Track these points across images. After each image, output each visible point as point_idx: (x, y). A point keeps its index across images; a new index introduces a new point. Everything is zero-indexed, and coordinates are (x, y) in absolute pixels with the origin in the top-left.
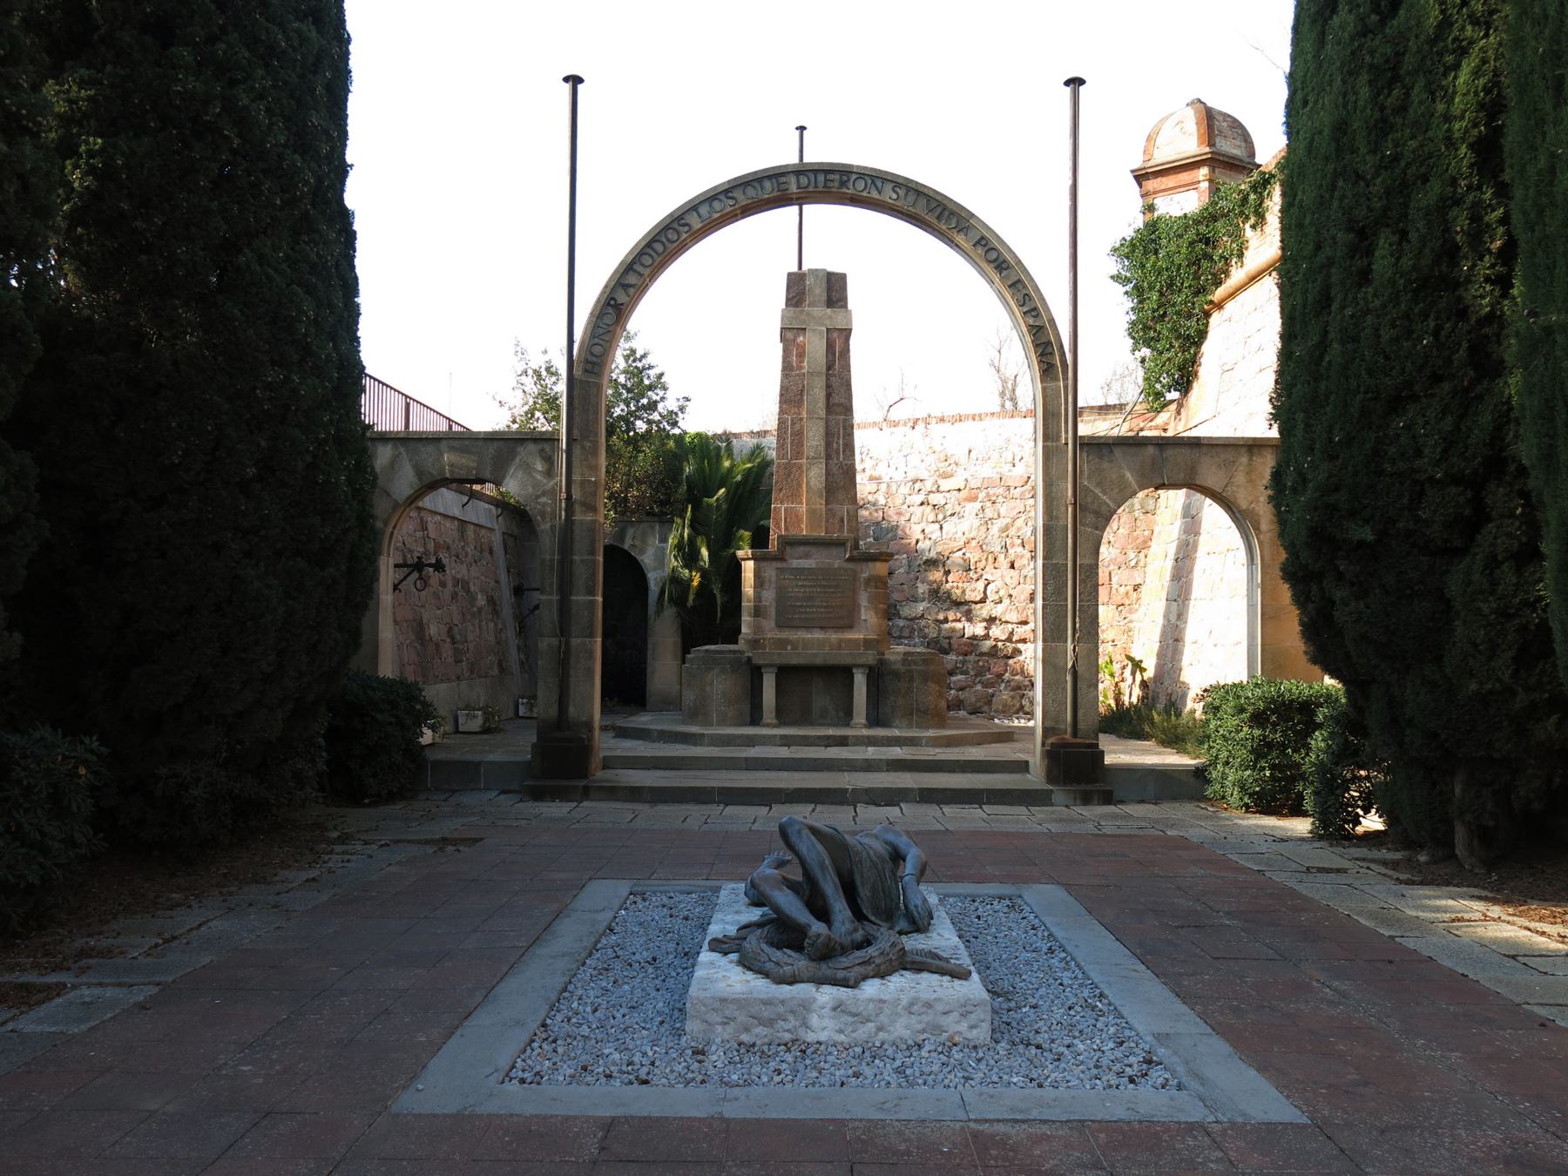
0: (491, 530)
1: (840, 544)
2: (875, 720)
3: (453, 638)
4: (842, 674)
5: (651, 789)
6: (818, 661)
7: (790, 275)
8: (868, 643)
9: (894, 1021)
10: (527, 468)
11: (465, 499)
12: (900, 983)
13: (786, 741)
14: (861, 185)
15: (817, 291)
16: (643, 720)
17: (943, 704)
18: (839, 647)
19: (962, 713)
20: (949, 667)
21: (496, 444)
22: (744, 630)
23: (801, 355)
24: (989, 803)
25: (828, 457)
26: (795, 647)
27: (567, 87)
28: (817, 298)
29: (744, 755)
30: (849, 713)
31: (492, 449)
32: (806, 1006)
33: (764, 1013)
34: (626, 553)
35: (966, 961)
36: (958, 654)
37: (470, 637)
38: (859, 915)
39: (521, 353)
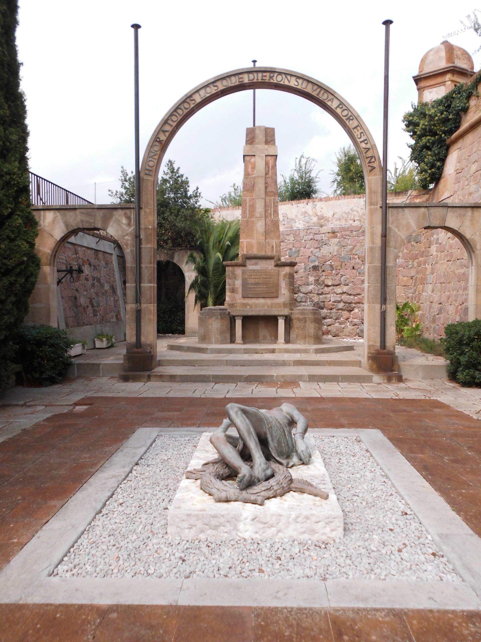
0: (111, 254)
1: (271, 258)
2: (287, 341)
4: (272, 320)
5: (180, 376)
6: (262, 313)
7: (247, 129)
8: (285, 305)
9: (287, 527)
10: (119, 223)
11: (98, 239)
12: (291, 498)
13: (246, 351)
14: (279, 78)
15: (261, 137)
16: (182, 341)
17: (321, 333)
18: (272, 307)
19: (330, 337)
20: (324, 315)
21: (103, 211)
22: (227, 299)
23: (253, 168)
24: (342, 382)
25: (266, 217)
26: (251, 307)
27: (133, 30)
28: (260, 138)
29: (225, 359)
30: (276, 337)
31: (101, 213)
32: (235, 520)
33: (212, 523)
34: (175, 265)
35: (327, 487)
36: (328, 309)
37: (102, 304)
38: (268, 457)
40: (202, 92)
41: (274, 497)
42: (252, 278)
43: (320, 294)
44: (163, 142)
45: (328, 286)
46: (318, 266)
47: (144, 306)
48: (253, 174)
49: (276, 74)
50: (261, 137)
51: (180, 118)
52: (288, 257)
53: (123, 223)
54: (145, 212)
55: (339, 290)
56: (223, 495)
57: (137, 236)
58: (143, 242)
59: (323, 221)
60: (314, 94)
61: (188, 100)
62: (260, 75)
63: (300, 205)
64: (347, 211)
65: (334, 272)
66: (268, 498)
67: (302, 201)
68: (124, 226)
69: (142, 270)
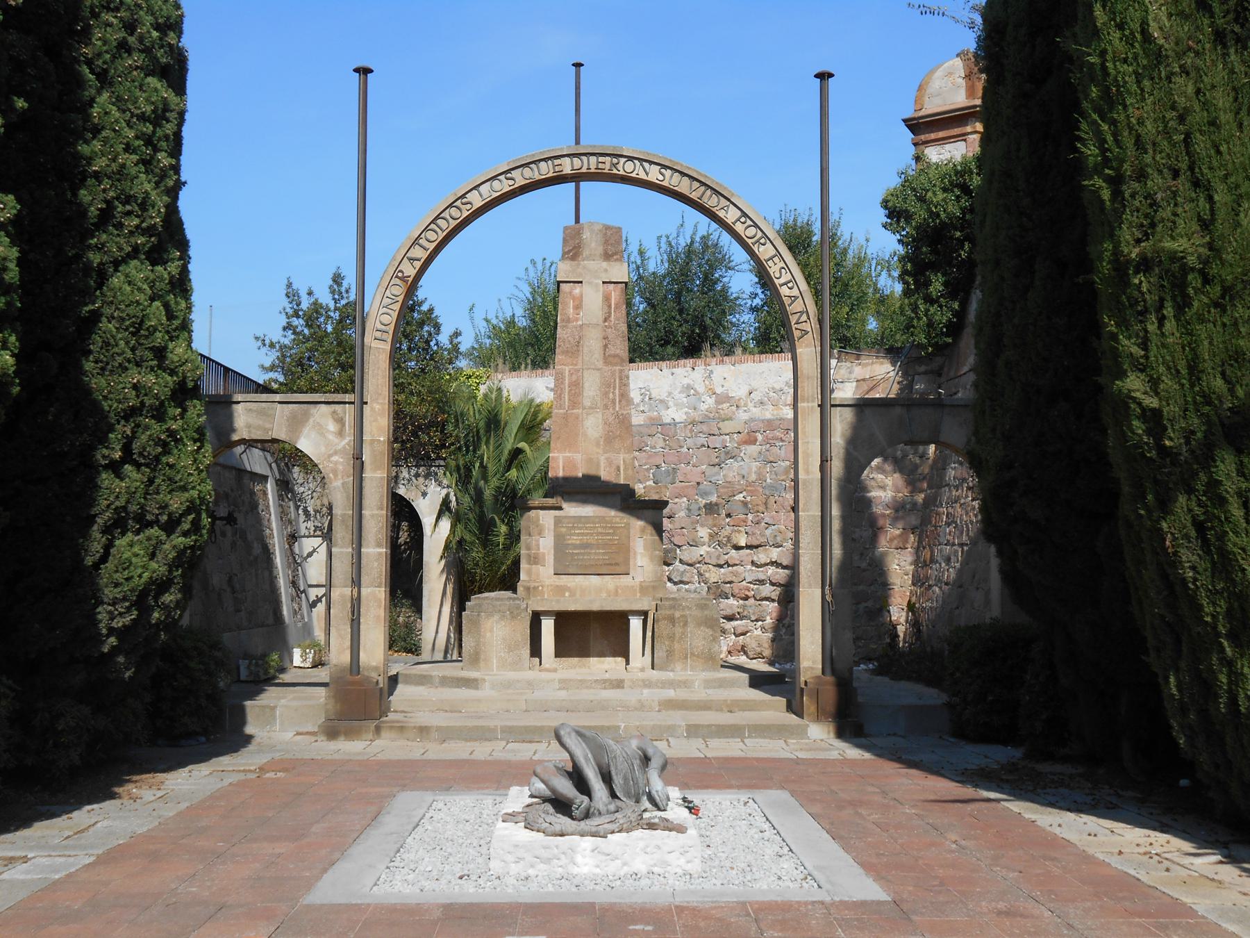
3: (233, 588)
6: (595, 607)
7: (566, 228)
8: (644, 589)
10: (320, 429)
26: (573, 594)
38: (613, 795)
39: (292, 295)
40: (485, 189)
41: (619, 831)
42: (575, 534)
43: (721, 566)
44: (410, 280)
45: (737, 548)
46: (716, 504)
47: (364, 591)
48: (577, 320)
49: (623, 160)
50: (593, 245)
51: (442, 235)
52: (651, 483)
53: (328, 431)
54: (372, 409)
55: (761, 557)
56: (557, 828)
57: (358, 458)
58: (367, 466)
59: (725, 406)
60: (694, 196)
61: (458, 203)
62: (593, 159)
63: (679, 371)
64: (777, 387)
65: (750, 517)
66: (613, 832)
67: (682, 362)
68: (331, 437)
69: (364, 522)
